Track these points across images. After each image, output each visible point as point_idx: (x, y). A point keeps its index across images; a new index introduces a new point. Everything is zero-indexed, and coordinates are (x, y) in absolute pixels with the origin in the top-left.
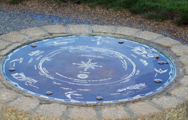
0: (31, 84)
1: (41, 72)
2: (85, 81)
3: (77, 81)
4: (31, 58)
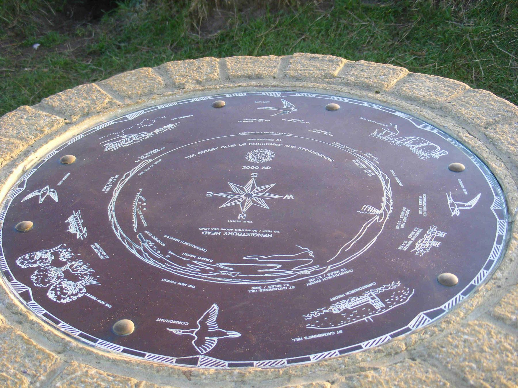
0: (385, 128)
1: (376, 164)
2: (252, 142)
3: (272, 142)
4: (403, 226)
